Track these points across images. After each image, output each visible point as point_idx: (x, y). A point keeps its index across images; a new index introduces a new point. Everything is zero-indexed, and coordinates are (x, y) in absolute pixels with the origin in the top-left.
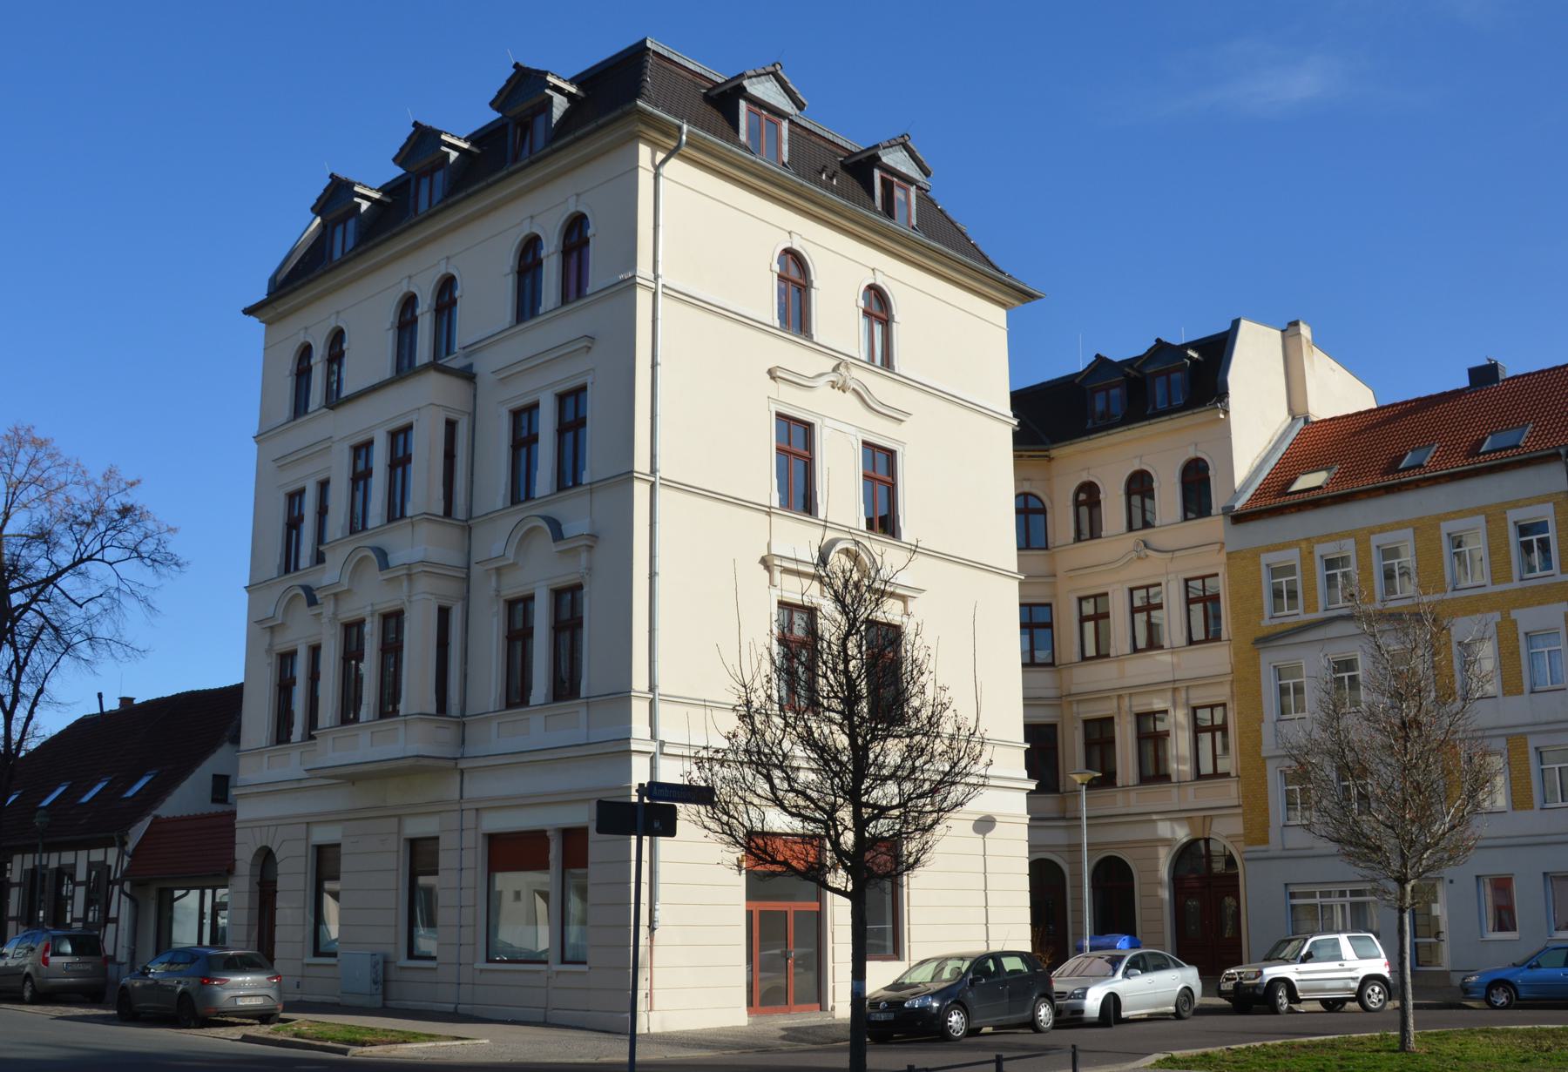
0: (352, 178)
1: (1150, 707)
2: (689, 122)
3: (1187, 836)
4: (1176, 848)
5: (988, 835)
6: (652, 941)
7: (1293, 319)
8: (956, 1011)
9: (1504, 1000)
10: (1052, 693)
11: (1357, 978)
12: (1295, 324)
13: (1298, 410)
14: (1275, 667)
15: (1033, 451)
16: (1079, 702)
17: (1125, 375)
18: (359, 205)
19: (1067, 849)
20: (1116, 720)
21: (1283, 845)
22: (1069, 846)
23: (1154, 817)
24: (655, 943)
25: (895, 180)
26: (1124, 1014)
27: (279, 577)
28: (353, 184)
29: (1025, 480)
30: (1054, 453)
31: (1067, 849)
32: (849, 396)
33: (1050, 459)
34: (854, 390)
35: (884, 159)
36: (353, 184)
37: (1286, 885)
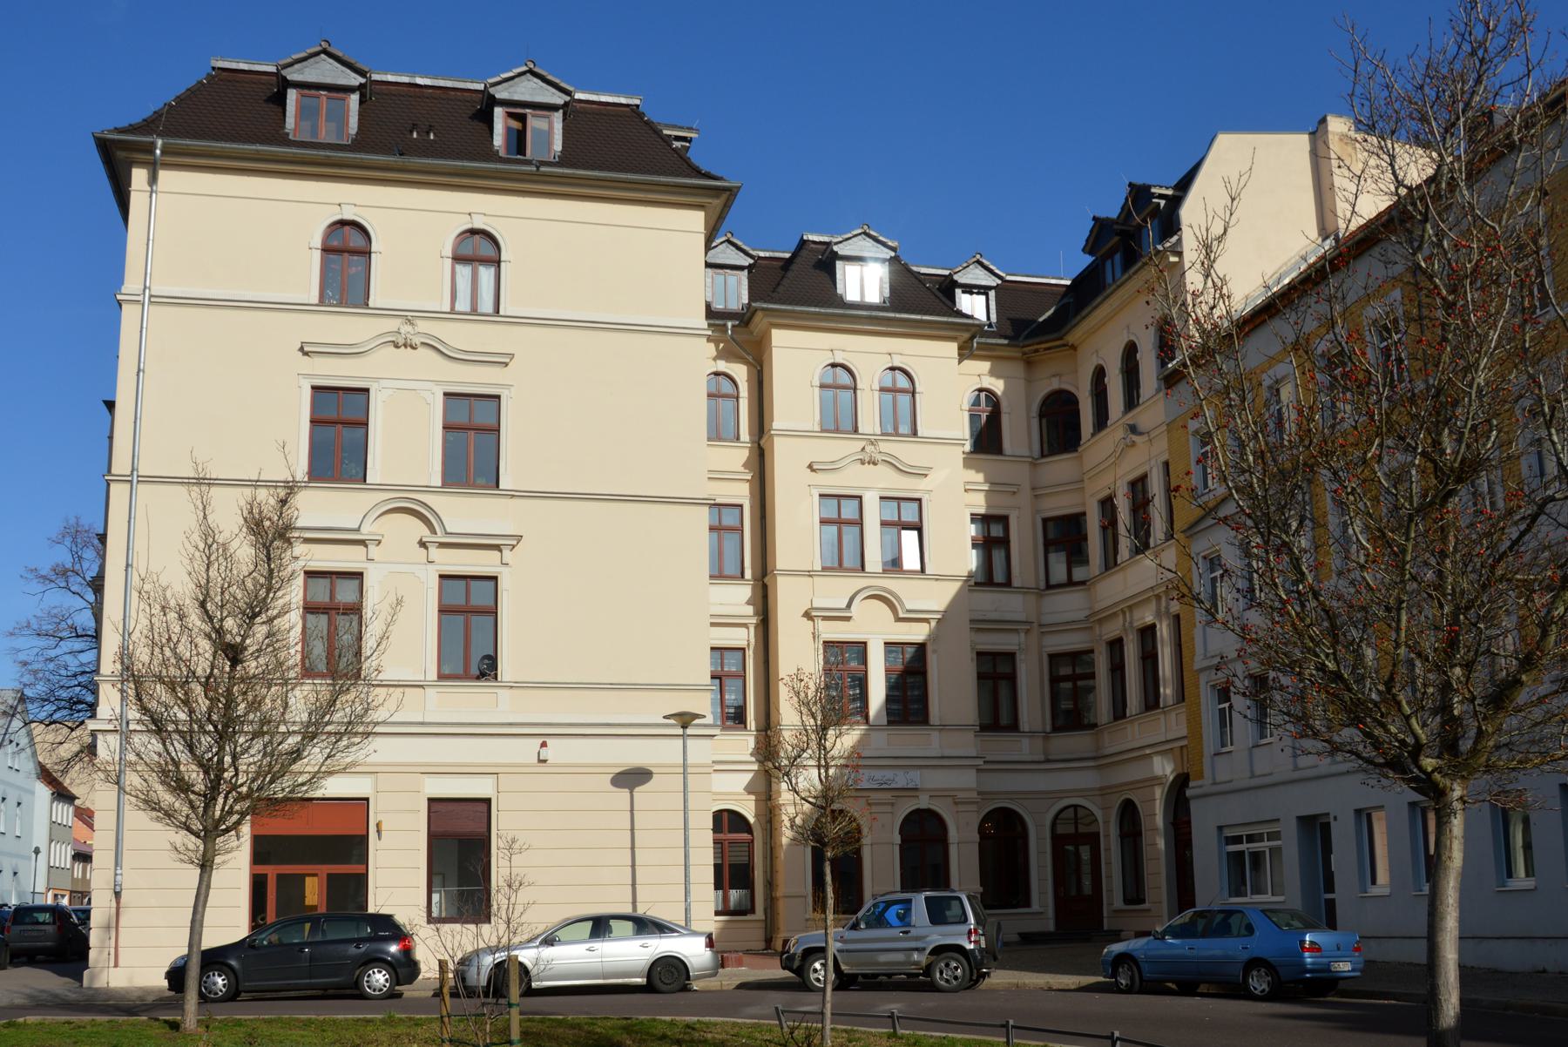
0: (1148, 182)
1: (1142, 622)
2: (159, 135)
3: (1172, 772)
4: (1168, 784)
5: (637, 789)
6: (118, 903)
7: (1320, 117)
8: (387, 976)
9: (1265, 986)
10: (1081, 615)
11: (924, 949)
12: (1323, 121)
13: (1330, 228)
14: (1205, 558)
15: (1047, 342)
16: (1100, 621)
17: (1117, 234)
18: (1159, 204)
19: (1097, 793)
20: (1125, 639)
21: (1214, 779)
22: (1101, 789)
23: (1148, 752)
24: (121, 905)
25: (528, 111)
26: (534, 985)
27: (1131, 558)
28: (1149, 187)
29: (1054, 376)
30: (1071, 338)
31: (1097, 793)
32: (422, 351)
33: (1074, 347)
34: (423, 343)
35: (497, 96)
36: (1149, 187)
37: (1220, 828)
